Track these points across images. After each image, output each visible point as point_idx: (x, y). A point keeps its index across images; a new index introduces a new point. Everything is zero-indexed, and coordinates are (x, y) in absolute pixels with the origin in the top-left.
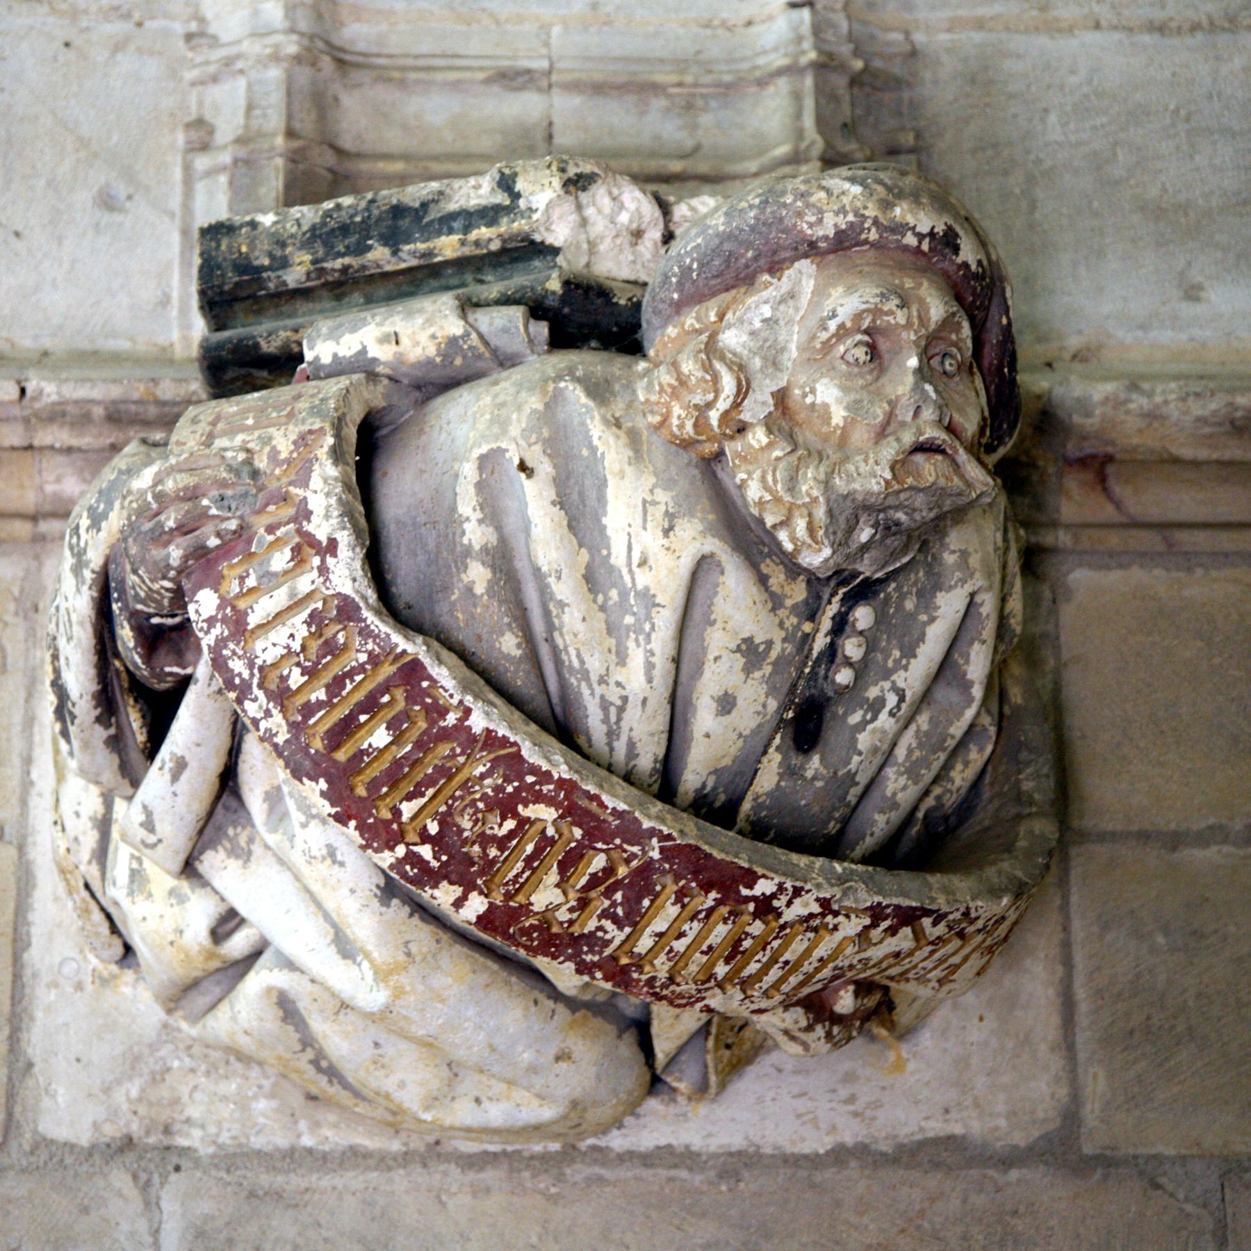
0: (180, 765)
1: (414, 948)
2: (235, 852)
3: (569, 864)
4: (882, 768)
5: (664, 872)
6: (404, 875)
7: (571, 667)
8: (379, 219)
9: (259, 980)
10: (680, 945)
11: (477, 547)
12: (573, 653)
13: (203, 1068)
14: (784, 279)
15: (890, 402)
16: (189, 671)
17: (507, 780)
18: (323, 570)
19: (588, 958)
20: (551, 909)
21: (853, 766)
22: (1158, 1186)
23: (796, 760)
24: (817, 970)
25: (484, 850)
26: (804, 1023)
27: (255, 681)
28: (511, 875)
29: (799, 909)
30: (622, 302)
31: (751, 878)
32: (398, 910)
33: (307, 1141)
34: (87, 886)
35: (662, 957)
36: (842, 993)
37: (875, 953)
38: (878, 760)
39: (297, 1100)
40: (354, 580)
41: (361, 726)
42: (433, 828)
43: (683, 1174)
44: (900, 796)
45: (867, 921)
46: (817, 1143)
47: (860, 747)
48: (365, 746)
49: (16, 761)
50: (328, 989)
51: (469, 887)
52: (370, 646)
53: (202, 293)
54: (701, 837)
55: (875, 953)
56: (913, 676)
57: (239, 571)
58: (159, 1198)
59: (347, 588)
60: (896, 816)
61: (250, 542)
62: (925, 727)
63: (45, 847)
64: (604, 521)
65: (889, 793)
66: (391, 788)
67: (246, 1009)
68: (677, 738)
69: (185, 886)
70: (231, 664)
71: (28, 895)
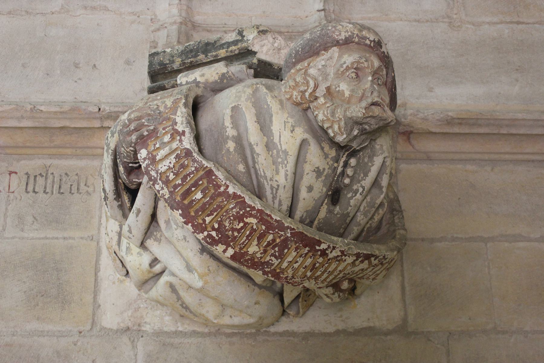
0: (139, 211)
1: (211, 268)
2: (156, 240)
3: (261, 238)
4: (356, 212)
5: (291, 241)
6: (207, 242)
7: (261, 175)
8: (202, 47)
9: (164, 279)
10: (296, 266)
11: (231, 136)
12: (262, 170)
13: (150, 307)
14: (329, 53)
15: (363, 90)
16: (141, 181)
17: (241, 210)
18: (181, 141)
19: (267, 270)
20: (255, 253)
21: (349, 210)
22: (429, 340)
23: (332, 208)
24: (339, 274)
25: (233, 233)
26: (332, 292)
27: (159, 178)
28: (241, 242)
29: (334, 254)
30: (276, 68)
31: (319, 243)
32: (206, 256)
33: (180, 329)
34: (115, 252)
35: (290, 269)
36: (344, 282)
37: (356, 269)
38: (356, 210)
39: (177, 317)
40: (191, 144)
41: (193, 192)
42: (216, 226)
43: (292, 338)
44: (361, 222)
45: (355, 258)
46: (331, 329)
47: (351, 204)
48: (194, 198)
49: (97, 217)
50: (185, 282)
51: (228, 245)
52: (195, 165)
53: (149, 73)
54: (304, 230)
55: (356, 269)
56: (367, 182)
57: (154, 143)
58: (137, 345)
59: (188, 146)
60: (360, 228)
61: (157, 133)
62: (369, 200)
63: (104, 241)
64: (272, 128)
65: (358, 221)
66: (202, 212)
67: (160, 288)
68: (294, 201)
69: (142, 251)
70: (151, 173)
71: (100, 256)
